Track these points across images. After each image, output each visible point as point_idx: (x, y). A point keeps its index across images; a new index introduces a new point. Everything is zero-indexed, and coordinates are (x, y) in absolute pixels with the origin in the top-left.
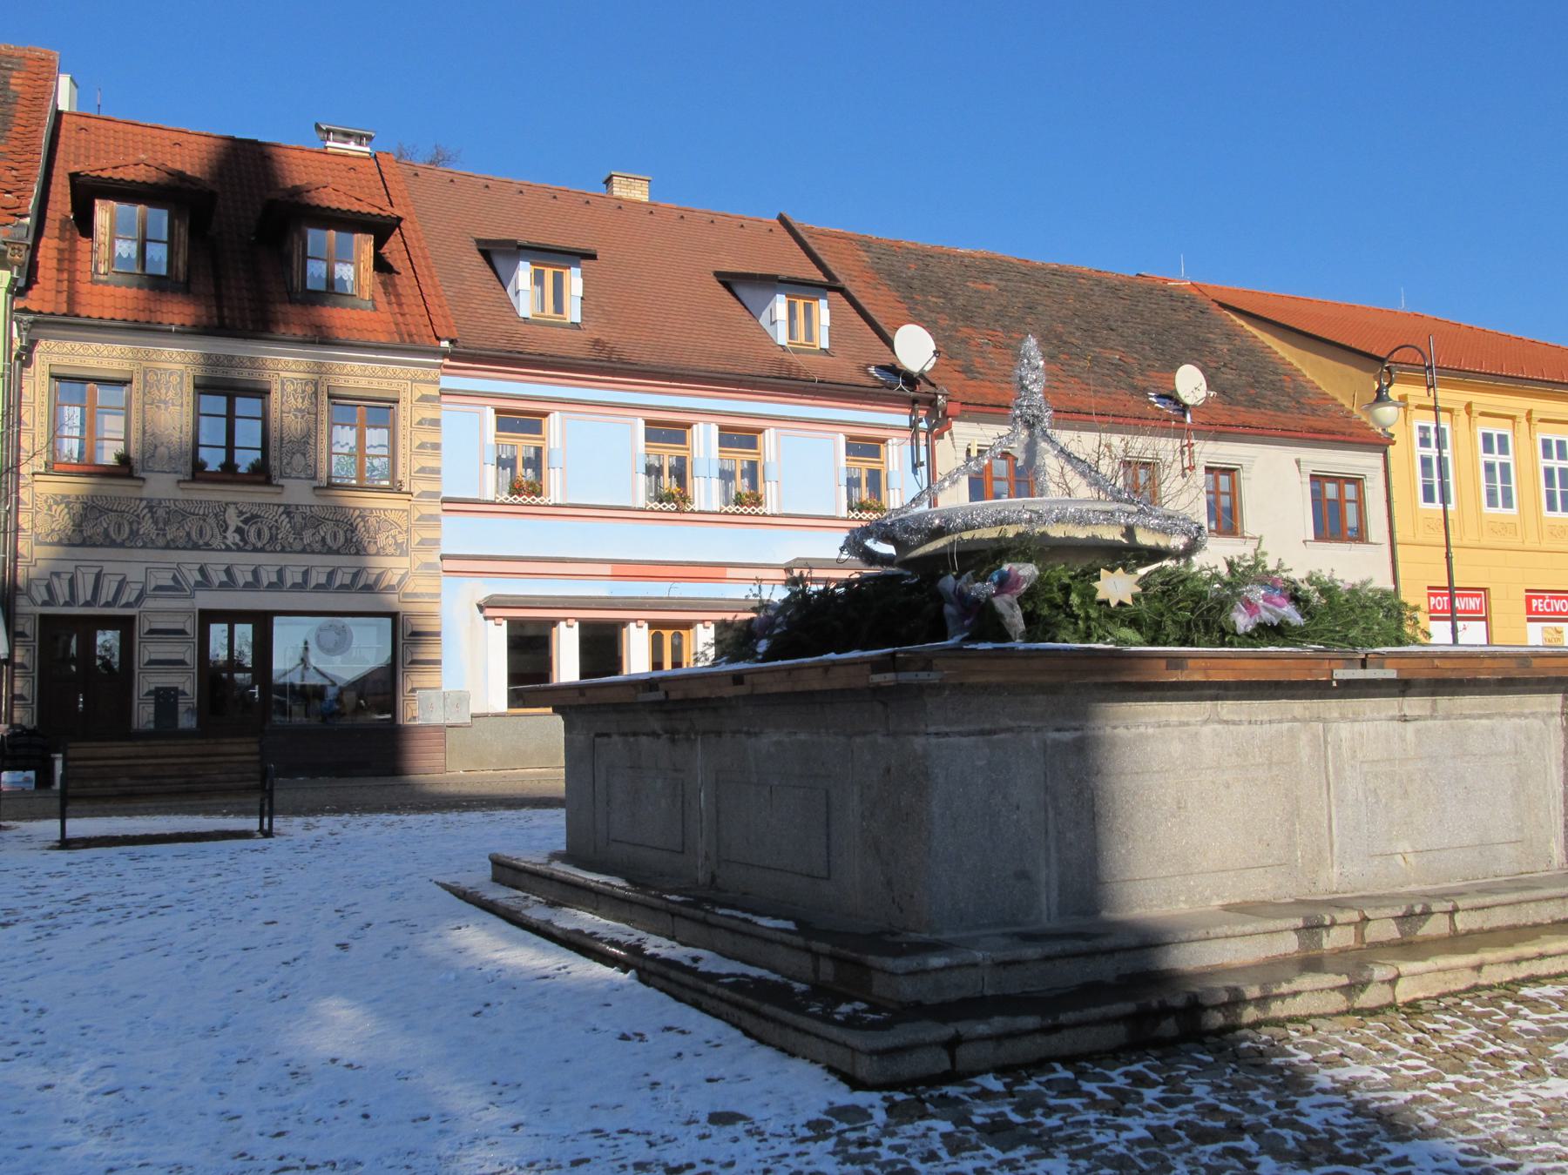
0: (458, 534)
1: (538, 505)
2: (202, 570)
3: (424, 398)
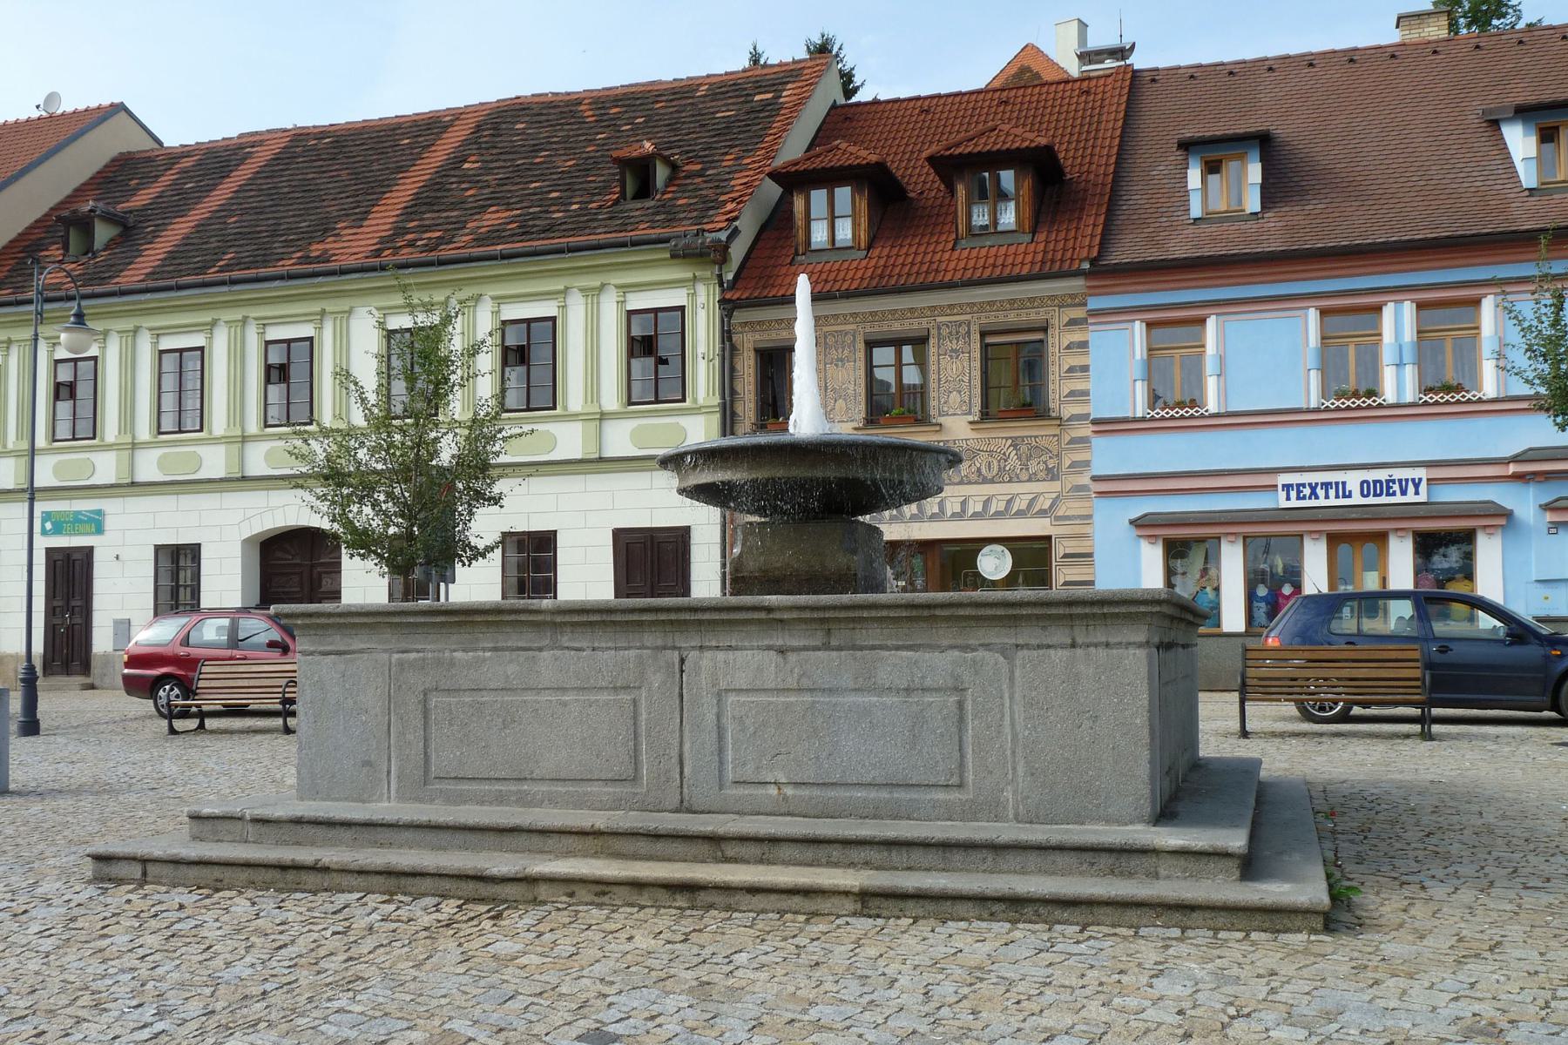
0: (1110, 455)
1: (1469, 401)
3: (1073, 322)
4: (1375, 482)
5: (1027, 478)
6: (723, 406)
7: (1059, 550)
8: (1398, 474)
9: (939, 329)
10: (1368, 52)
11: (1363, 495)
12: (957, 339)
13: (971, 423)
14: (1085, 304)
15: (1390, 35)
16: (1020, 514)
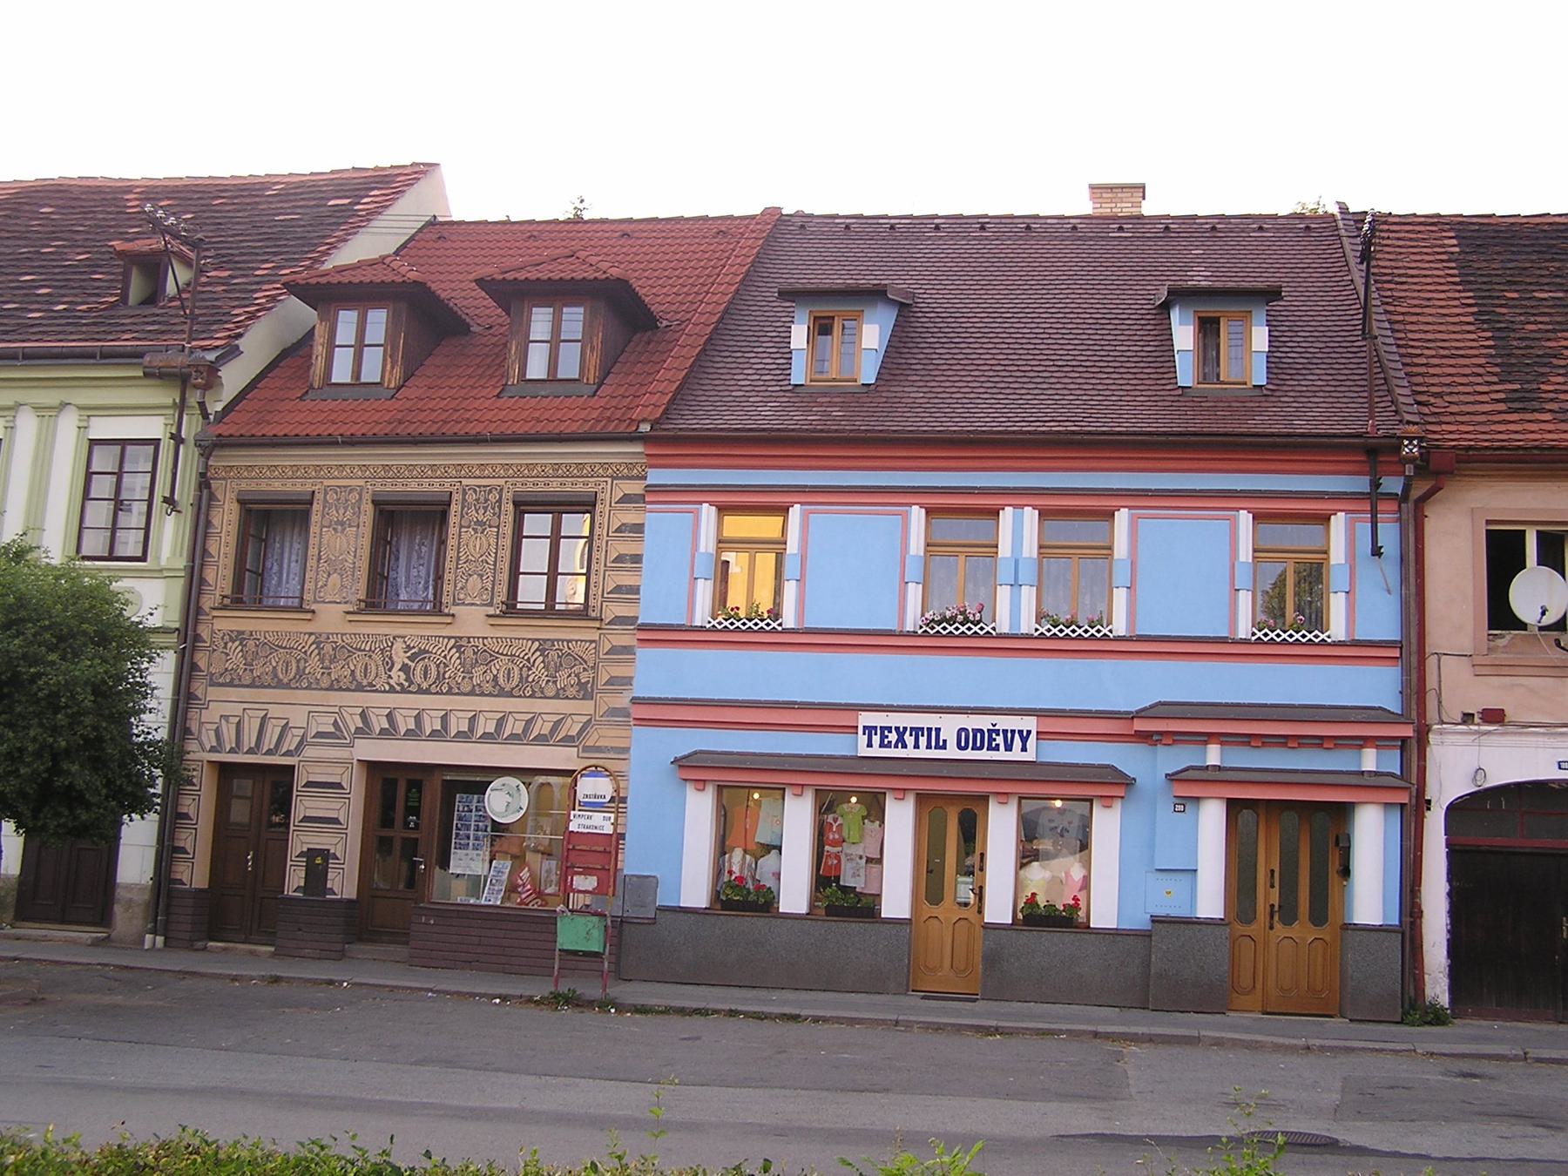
2: (363, 715)
3: (626, 499)
4: (975, 731)
5: (469, 688)
6: (191, 570)
7: (300, 779)
8: (1005, 723)
9: (465, 493)
10: (1049, 221)
11: (960, 747)
12: (485, 509)
13: (489, 616)
14: (645, 478)
15: (1082, 205)
16: (542, 740)
